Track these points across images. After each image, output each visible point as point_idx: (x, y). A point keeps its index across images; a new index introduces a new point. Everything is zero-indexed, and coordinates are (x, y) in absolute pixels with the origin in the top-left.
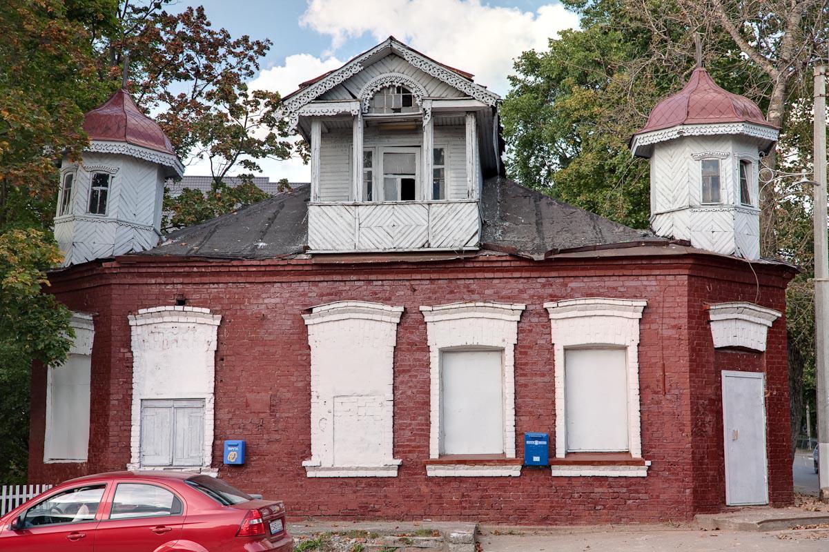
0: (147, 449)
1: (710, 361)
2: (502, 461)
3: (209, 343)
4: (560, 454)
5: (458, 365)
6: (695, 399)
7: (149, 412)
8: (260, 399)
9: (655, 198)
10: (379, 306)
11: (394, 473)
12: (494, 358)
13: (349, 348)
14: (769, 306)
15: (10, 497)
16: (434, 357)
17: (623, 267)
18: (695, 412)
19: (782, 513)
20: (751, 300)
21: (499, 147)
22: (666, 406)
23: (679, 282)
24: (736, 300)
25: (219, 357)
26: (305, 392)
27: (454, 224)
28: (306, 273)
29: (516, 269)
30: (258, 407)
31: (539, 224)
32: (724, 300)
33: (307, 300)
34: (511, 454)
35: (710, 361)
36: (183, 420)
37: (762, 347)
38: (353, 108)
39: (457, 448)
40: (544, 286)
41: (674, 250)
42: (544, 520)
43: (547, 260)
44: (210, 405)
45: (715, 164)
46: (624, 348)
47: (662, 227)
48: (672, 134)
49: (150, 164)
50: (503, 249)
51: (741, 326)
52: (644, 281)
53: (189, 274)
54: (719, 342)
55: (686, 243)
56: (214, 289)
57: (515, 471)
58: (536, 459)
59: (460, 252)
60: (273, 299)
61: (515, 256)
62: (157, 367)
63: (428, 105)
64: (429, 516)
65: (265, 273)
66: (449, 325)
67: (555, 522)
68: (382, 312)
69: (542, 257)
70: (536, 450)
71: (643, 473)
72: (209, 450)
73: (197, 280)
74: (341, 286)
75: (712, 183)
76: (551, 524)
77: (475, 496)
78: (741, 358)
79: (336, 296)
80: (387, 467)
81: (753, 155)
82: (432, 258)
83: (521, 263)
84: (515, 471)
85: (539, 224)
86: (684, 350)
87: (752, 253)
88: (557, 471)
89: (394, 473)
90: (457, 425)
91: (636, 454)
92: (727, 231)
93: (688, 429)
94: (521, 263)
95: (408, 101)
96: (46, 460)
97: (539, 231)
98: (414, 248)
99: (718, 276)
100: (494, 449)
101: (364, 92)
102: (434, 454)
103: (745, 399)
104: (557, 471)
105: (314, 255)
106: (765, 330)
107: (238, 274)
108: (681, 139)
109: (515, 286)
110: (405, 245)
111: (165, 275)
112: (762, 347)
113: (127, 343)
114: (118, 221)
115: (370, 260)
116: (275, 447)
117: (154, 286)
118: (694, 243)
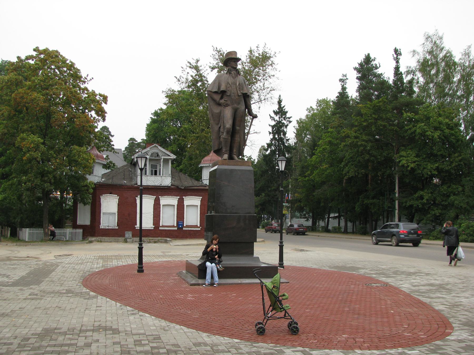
4: (185, 225)
27: (167, 181)
34: (175, 225)
44: (117, 214)
63: (163, 157)
66: (164, 200)
80: (152, 227)
85: (180, 179)
88: (184, 229)
91: (199, 226)
95: (158, 155)
98: (159, 185)
101: (150, 154)
102: (161, 225)
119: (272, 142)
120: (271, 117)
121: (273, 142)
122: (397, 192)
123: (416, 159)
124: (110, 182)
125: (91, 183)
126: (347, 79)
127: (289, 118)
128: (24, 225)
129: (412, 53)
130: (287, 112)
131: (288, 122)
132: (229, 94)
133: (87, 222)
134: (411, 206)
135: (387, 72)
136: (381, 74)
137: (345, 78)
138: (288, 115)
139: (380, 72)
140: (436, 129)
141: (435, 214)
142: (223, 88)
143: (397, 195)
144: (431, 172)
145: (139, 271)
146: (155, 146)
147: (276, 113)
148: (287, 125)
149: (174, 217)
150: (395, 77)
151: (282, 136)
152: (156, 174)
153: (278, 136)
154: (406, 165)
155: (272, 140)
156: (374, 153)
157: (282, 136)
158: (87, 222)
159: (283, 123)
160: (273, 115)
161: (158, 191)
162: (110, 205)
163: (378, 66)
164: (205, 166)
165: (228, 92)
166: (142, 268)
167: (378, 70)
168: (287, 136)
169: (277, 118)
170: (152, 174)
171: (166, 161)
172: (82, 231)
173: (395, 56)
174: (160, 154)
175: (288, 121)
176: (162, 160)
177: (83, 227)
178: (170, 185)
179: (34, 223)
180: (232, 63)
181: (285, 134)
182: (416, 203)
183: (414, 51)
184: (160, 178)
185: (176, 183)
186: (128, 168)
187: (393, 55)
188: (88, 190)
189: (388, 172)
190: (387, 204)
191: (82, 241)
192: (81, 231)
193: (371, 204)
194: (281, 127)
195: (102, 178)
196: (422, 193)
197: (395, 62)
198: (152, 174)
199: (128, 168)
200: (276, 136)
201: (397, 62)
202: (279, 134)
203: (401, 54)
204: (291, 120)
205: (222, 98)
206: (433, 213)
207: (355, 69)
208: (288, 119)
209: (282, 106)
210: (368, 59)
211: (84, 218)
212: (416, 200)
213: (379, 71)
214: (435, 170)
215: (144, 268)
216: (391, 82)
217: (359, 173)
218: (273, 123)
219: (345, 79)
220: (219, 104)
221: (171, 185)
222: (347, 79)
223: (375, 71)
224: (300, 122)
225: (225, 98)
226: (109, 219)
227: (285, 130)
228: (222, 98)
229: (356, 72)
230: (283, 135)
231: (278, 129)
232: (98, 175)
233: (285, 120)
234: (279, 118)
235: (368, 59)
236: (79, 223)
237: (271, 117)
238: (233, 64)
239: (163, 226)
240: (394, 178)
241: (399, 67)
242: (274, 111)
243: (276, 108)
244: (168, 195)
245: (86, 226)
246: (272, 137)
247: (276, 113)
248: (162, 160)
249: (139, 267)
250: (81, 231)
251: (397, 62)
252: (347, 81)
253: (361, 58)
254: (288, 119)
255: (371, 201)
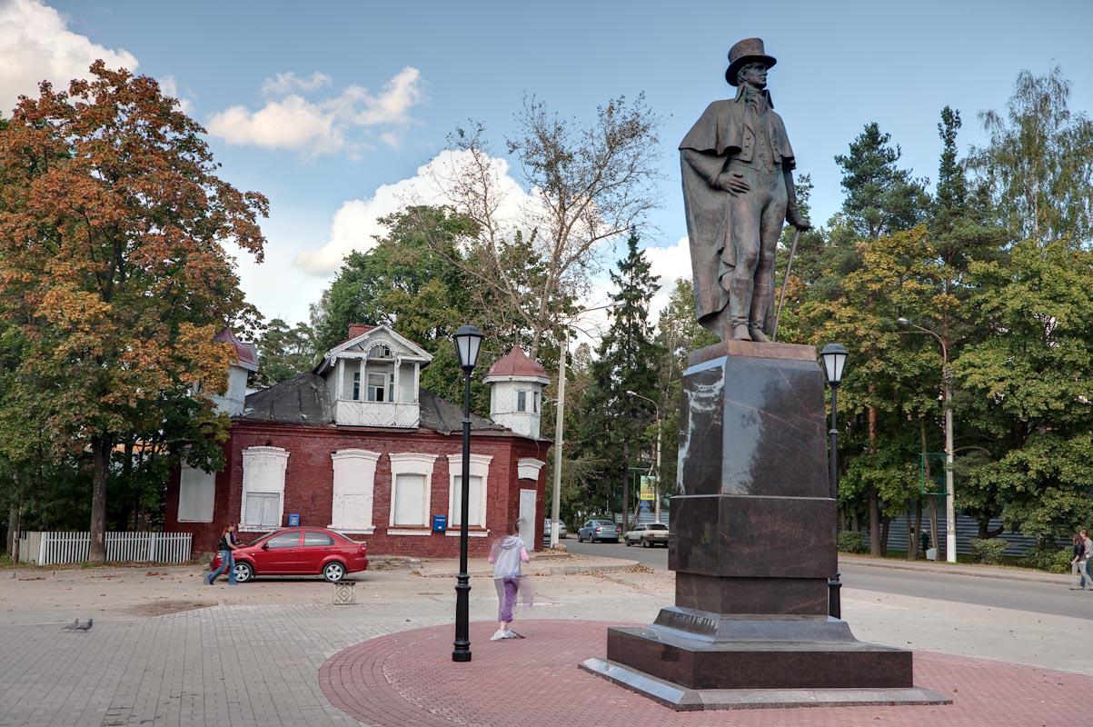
0: (249, 517)
1: (517, 484)
2: (423, 528)
3: (283, 466)
4: (450, 526)
5: (405, 482)
6: (510, 501)
7: (250, 498)
8: (307, 494)
9: (495, 406)
10: (369, 452)
11: (372, 533)
12: (420, 480)
13: (353, 474)
14: (540, 459)
15: (168, 539)
16: (394, 477)
17: (483, 440)
18: (509, 508)
19: (542, 554)
20: (534, 456)
21: (904, 652)
22: (498, 505)
23: (507, 448)
24: (528, 457)
25: (287, 473)
26: (330, 493)
27: (406, 413)
28: (332, 434)
29: (434, 438)
30: (305, 498)
31: (439, 413)
32: (524, 457)
33: (333, 447)
34: (427, 525)
35: (517, 484)
36: (267, 504)
37: (536, 479)
38: (364, 356)
39: (401, 522)
40: (446, 447)
41: (505, 434)
42: (441, 556)
43: (451, 435)
44: (282, 497)
45: (524, 393)
46: (481, 477)
47: (498, 420)
48: (507, 378)
49: (244, 369)
50: (429, 428)
51: (529, 469)
52: (492, 447)
53: (273, 431)
54: (520, 476)
55: (509, 430)
56: (285, 439)
57: (428, 533)
58: (440, 528)
59: (410, 429)
60: (313, 446)
61: (436, 433)
62: (256, 476)
63: (400, 358)
64: (386, 553)
65: (312, 433)
66: (402, 463)
67: (445, 557)
68: (370, 455)
69: (448, 434)
70: (440, 524)
71: (486, 535)
72: (281, 519)
73: (278, 433)
74: (350, 441)
75: (522, 407)
76: (1018, 665)
77: (409, 544)
78: (528, 483)
79: (349, 446)
80: (369, 530)
81: (539, 390)
82: (396, 431)
83: (437, 436)
84: (428, 533)
85: (439, 413)
86: (507, 479)
87: (536, 436)
88: (448, 534)
89: (372, 533)
90: (401, 511)
91: (484, 527)
92: (526, 426)
93: (506, 516)
94: (437, 436)
95: (387, 353)
96: (179, 520)
97: (440, 418)
98: (389, 425)
99: (523, 447)
100: (419, 523)
101: (367, 348)
102: (391, 524)
103: (528, 499)
104: (448, 534)
105: (338, 426)
106: (538, 470)
107: (299, 432)
108: (510, 381)
109: (433, 446)
110: (384, 424)
111: (262, 430)
112: (536, 479)
113: (240, 463)
114: (231, 400)
115: (367, 430)
116: (313, 518)
117: (255, 435)
118: (513, 430)
119: (613, 334)
120: (613, 276)
121: (616, 334)
122: (951, 452)
123: (1007, 372)
124: (266, 415)
125: (222, 417)
126: (811, 186)
127: (654, 279)
128: (31, 523)
129: (985, 118)
130: (649, 266)
131: (651, 289)
132: (747, 158)
133: (206, 516)
134: (994, 487)
135: (920, 165)
136: (904, 172)
137: (807, 184)
138: (652, 272)
139: (900, 168)
140: (1057, 298)
141: (1059, 508)
142: (731, 141)
143: (950, 459)
144: (1047, 404)
145: (456, 658)
146: (382, 330)
147: (624, 267)
148: (650, 296)
149: (424, 506)
150: (942, 177)
151: (638, 321)
152: (380, 398)
153: (629, 320)
154: (981, 386)
155: (613, 328)
156: (894, 355)
157: (638, 321)
158: (206, 516)
159: (642, 291)
160: (617, 271)
161: (386, 439)
162: (265, 472)
163: (896, 153)
164: (501, 382)
165: (745, 150)
166: (466, 647)
167: (896, 163)
168: (648, 319)
169: (626, 278)
170: (371, 399)
171: (407, 366)
172: (189, 538)
173: (945, 127)
174: (394, 349)
175: (651, 285)
176: (397, 366)
177: (195, 529)
178: (416, 426)
179: (66, 517)
180: (752, 71)
181: (644, 315)
182: (1006, 479)
183: (990, 115)
184: (393, 407)
185: (433, 422)
186: (308, 382)
187: (940, 125)
188: (213, 435)
189: (929, 404)
190: (925, 484)
191: (188, 564)
192: (186, 538)
193: (880, 481)
194: (638, 298)
195: (246, 406)
196: (1020, 454)
197: (943, 142)
198: (371, 399)
199: (308, 382)
200: (624, 321)
201: (949, 142)
202: (630, 316)
203: (959, 124)
204: (658, 283)
205: (725, 169)
206: (1054, 504)
207: (839, 160)
208: (651, 282)
209: (638, 252)
210: (873, 137)
211: (197, 501)
212: (1009, 471)
213: (900, 165)
214: (1057, 399)
215: (471, 649)
216: (932, 191)
217: (855, 406)
218: (617, 290)
219: (806, 188)
220: (716, 188)
221: (420, 426)
222: (811, 186)
223: (890, 166)
224: (682, 287)
225: (737, 168)
226: (262, 509)
227: (645, 307)
228: (725, 169)
229: (841, 167)
230: (641, 317)
231: (630, 302)
232: (233, 401)
233: (644, 283)
234: (632, 278)
235: (873, 137)
236: (183, 516)
237: (613, 276)
238: (754, 74)
239: (396, 527)
240: (942, 419)
241: (955, 155)
242: (620, 264)
243: (624, 254)
244: (413, 449)
245: (202, 525)
246: (614, 323)
247: (624, 267)
248: (397, 366)
249: (457, 647)
250: (186, 538)
251: (949, 142)
252: (811, 191)
253: (856, 133)
254: (651, 282)
255: (878, 474)
